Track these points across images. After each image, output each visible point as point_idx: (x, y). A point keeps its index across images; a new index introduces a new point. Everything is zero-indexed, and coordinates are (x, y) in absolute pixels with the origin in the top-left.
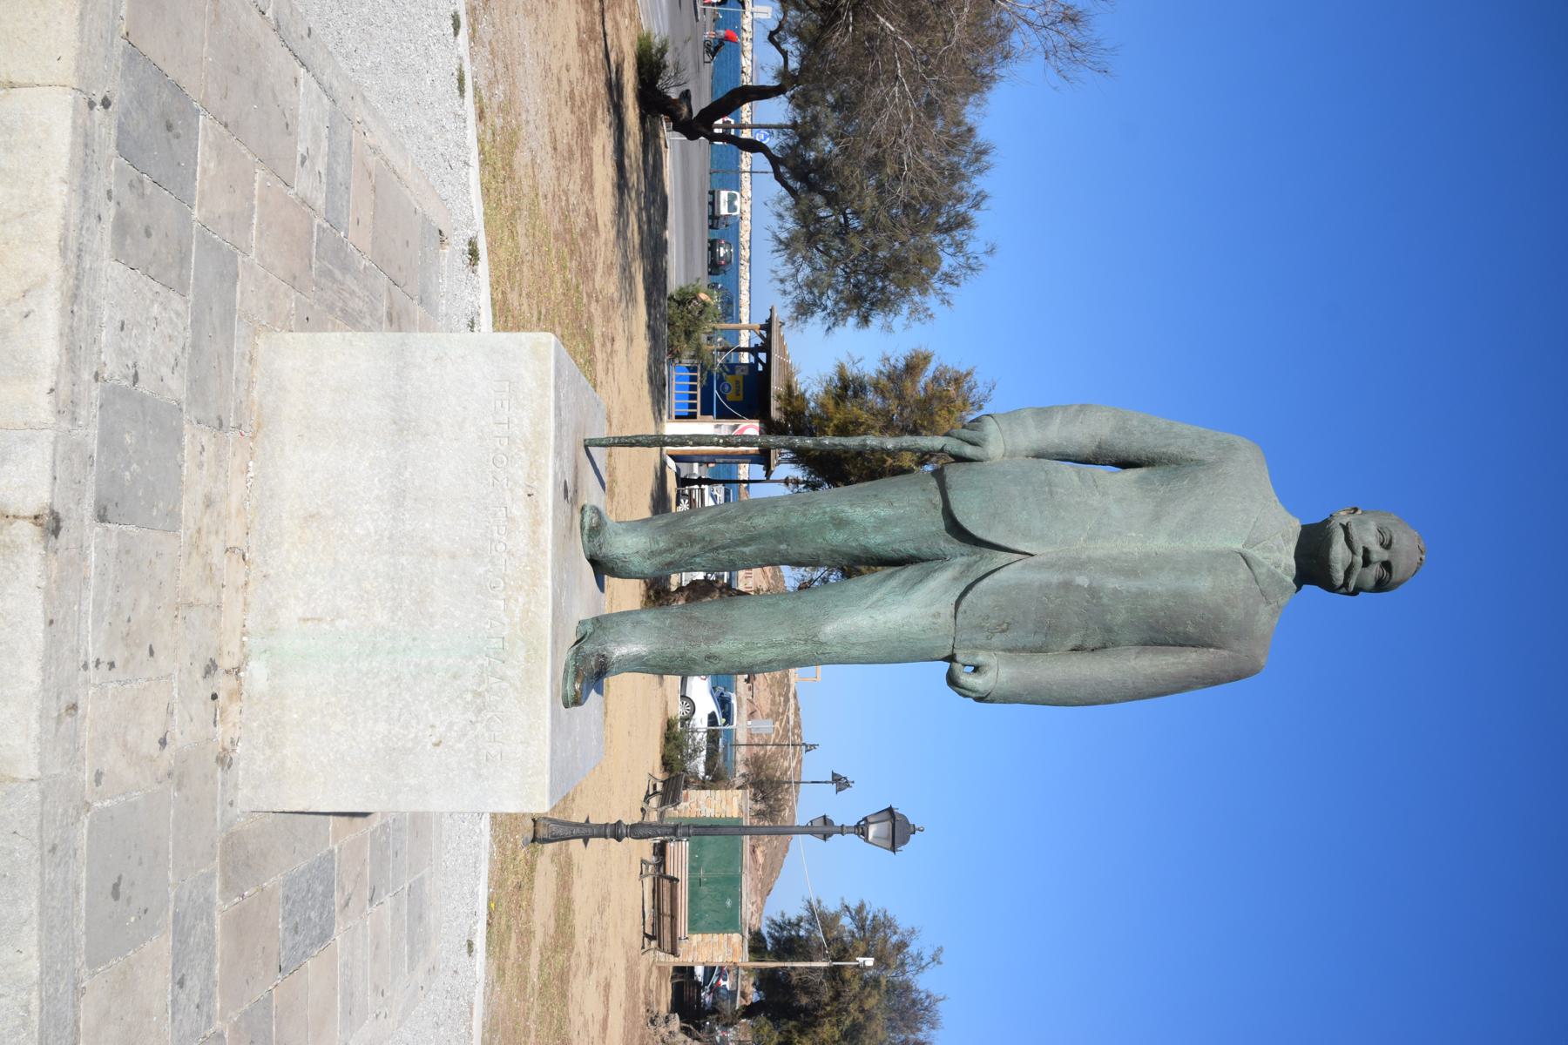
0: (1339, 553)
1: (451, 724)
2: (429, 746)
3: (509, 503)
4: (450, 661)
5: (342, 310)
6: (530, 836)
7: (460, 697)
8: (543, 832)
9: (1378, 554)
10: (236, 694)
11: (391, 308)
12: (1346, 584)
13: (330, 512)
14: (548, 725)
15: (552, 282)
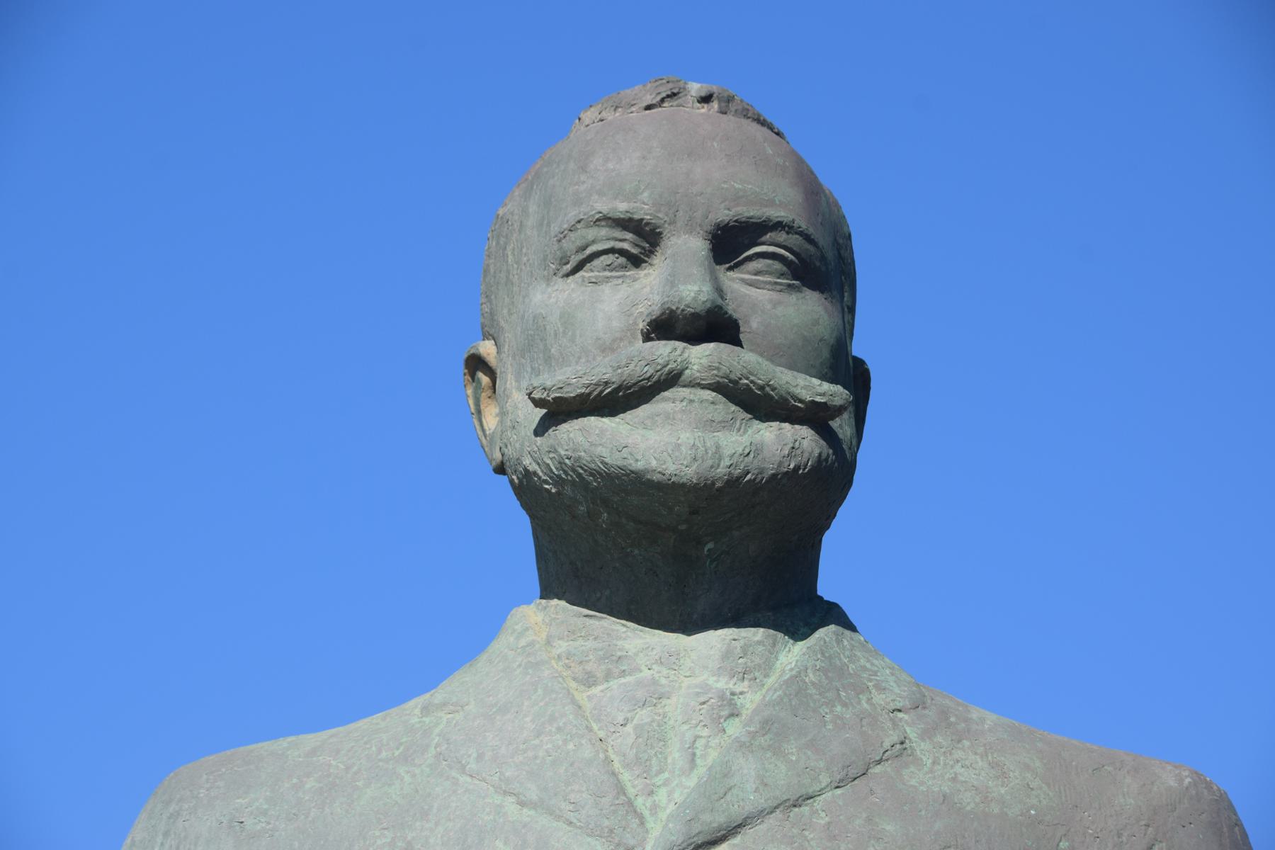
0: (673, 441)
9: (678, 275)
12: (815, 416)
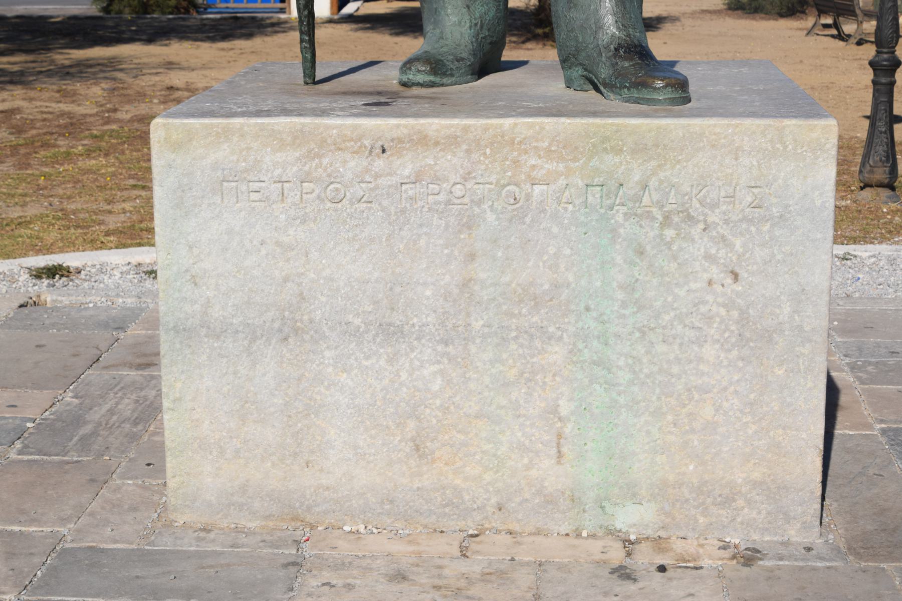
1: (708, 257)
2: (738, 288)
3: (395, 180)
4: (619, 260)
5: (136, 423)
6: (885, 193)
7: (669, 245)
8: (881, 174)
10: (659, 543)
11: (131, 366)
13: (412, 424)
14: (712, 121)
15: (89, 171)
